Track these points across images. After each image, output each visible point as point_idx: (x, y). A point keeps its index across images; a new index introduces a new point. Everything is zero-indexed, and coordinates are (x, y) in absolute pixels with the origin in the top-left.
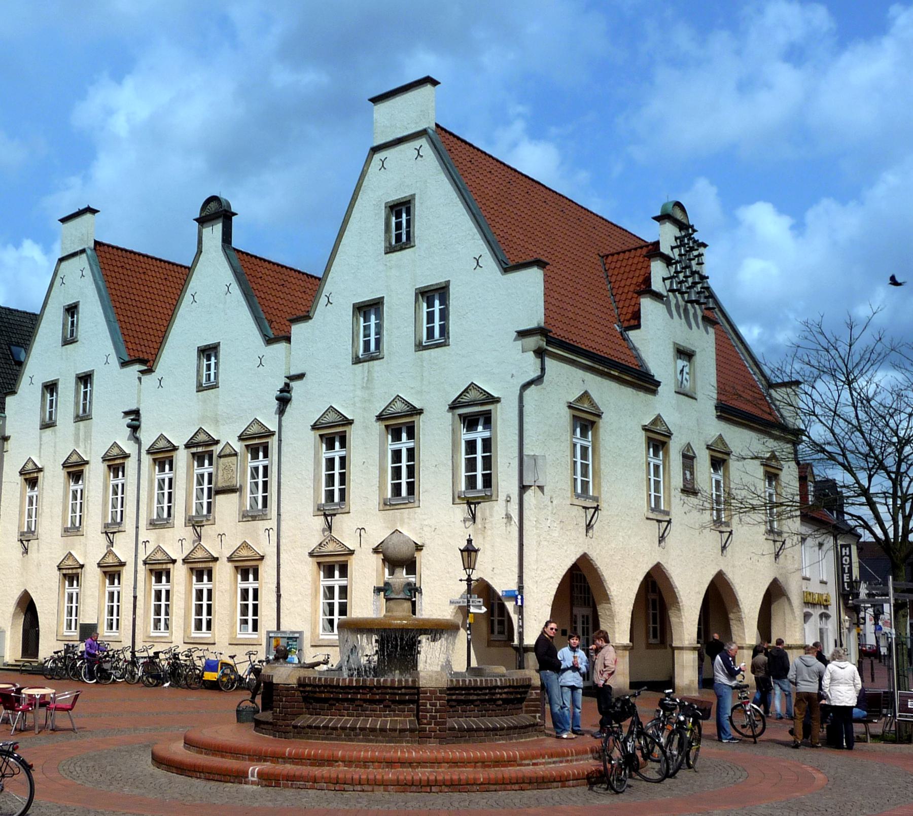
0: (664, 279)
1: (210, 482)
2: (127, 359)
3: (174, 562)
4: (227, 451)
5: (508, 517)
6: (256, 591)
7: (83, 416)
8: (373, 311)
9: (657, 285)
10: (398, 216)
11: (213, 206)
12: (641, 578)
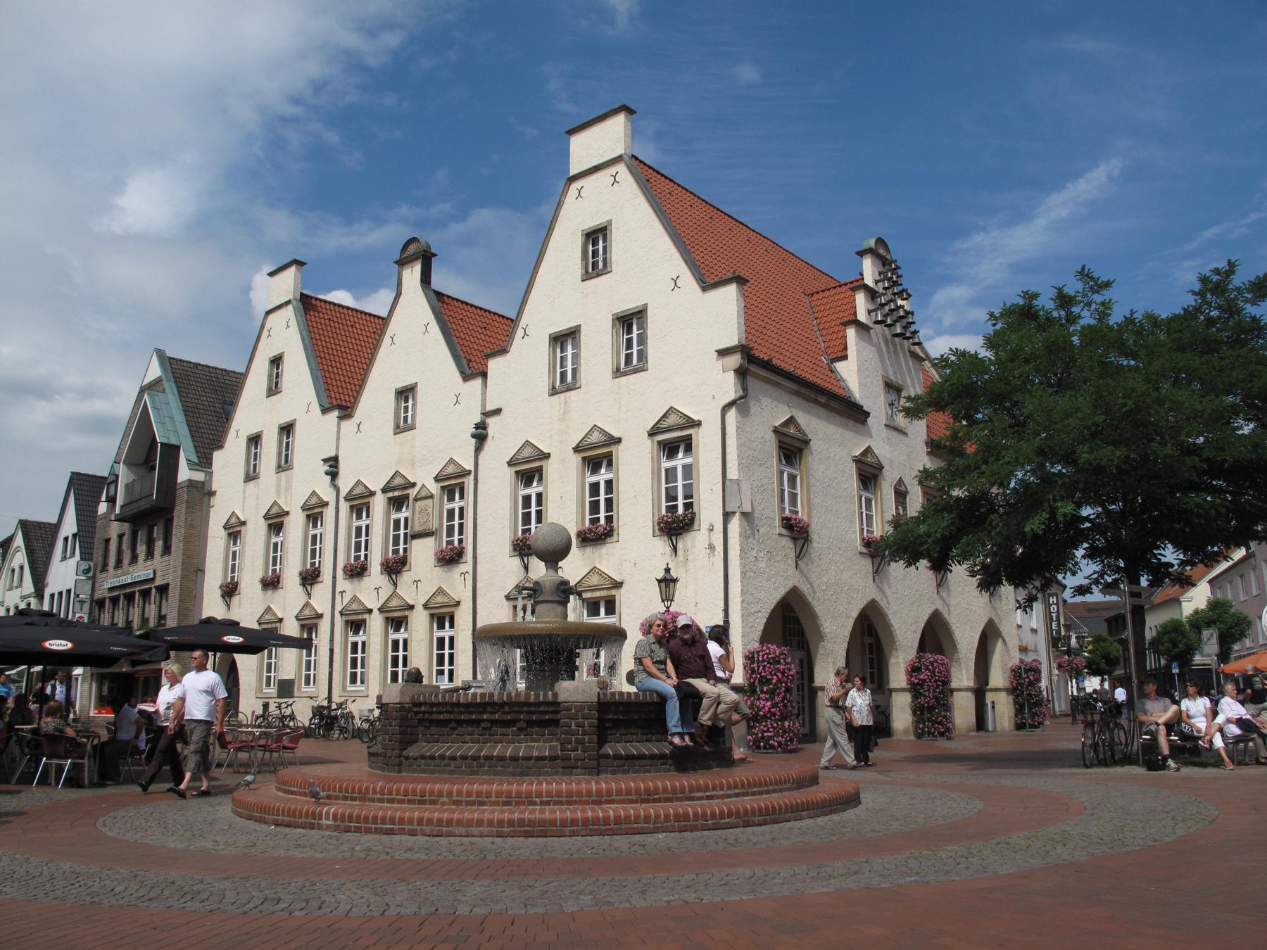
1: (406, 528)
2: (327, 406)
3: (370, 611)
4: (423, 494)
5: (712, 547)
6: (452, 639)
7: (284, 464)
8: (570, 341)
10: (595, 243)
11: (412, 248)
12: (855, 615)
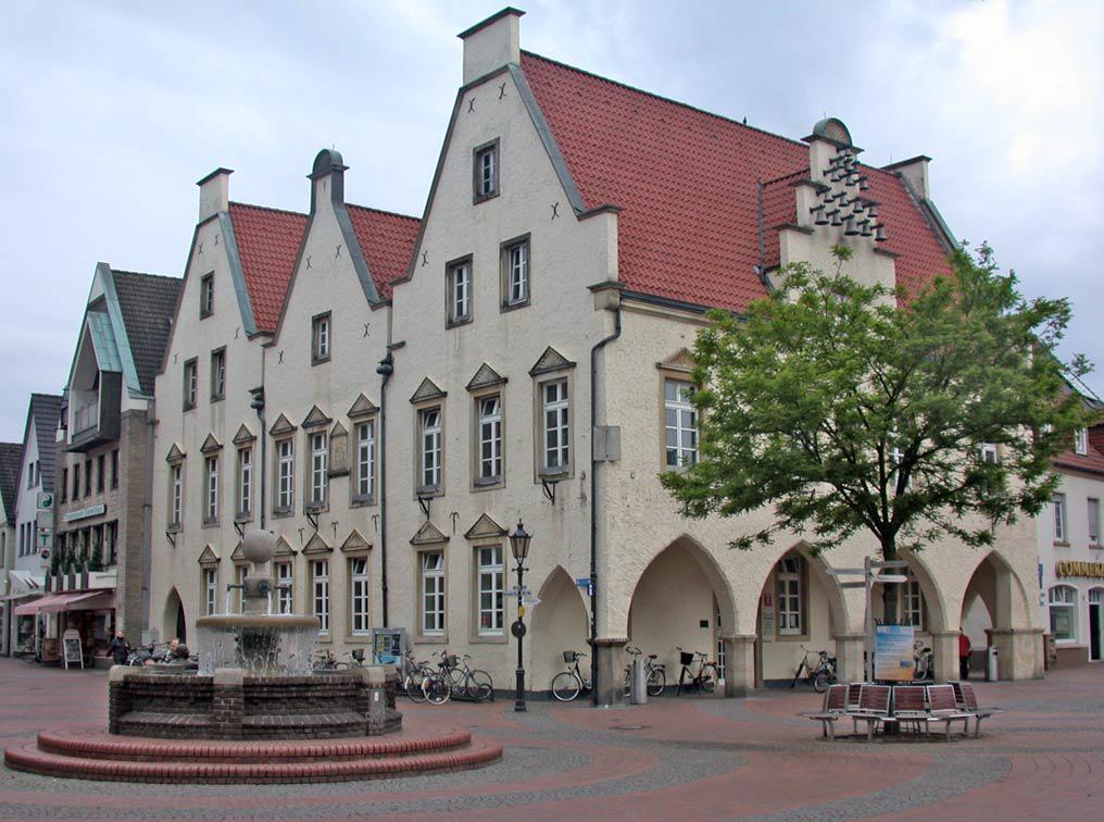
0: (812, 211)
7: (217, 397)
9: (804, 218)
